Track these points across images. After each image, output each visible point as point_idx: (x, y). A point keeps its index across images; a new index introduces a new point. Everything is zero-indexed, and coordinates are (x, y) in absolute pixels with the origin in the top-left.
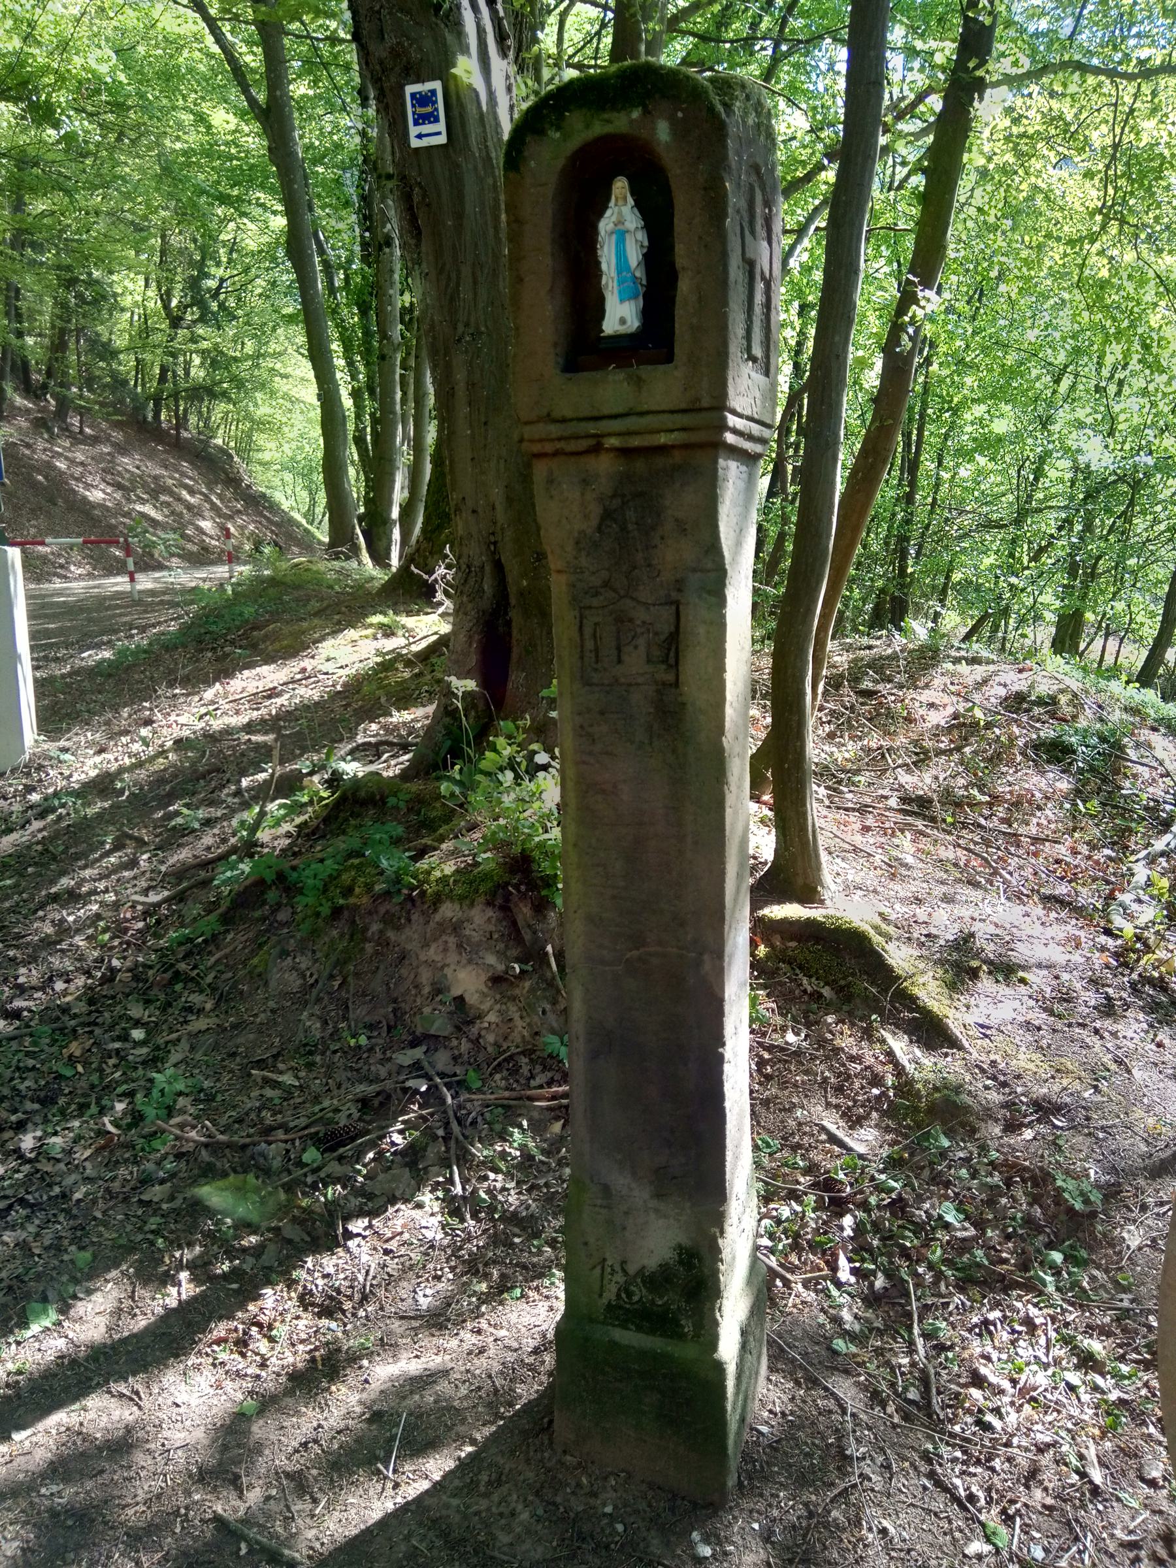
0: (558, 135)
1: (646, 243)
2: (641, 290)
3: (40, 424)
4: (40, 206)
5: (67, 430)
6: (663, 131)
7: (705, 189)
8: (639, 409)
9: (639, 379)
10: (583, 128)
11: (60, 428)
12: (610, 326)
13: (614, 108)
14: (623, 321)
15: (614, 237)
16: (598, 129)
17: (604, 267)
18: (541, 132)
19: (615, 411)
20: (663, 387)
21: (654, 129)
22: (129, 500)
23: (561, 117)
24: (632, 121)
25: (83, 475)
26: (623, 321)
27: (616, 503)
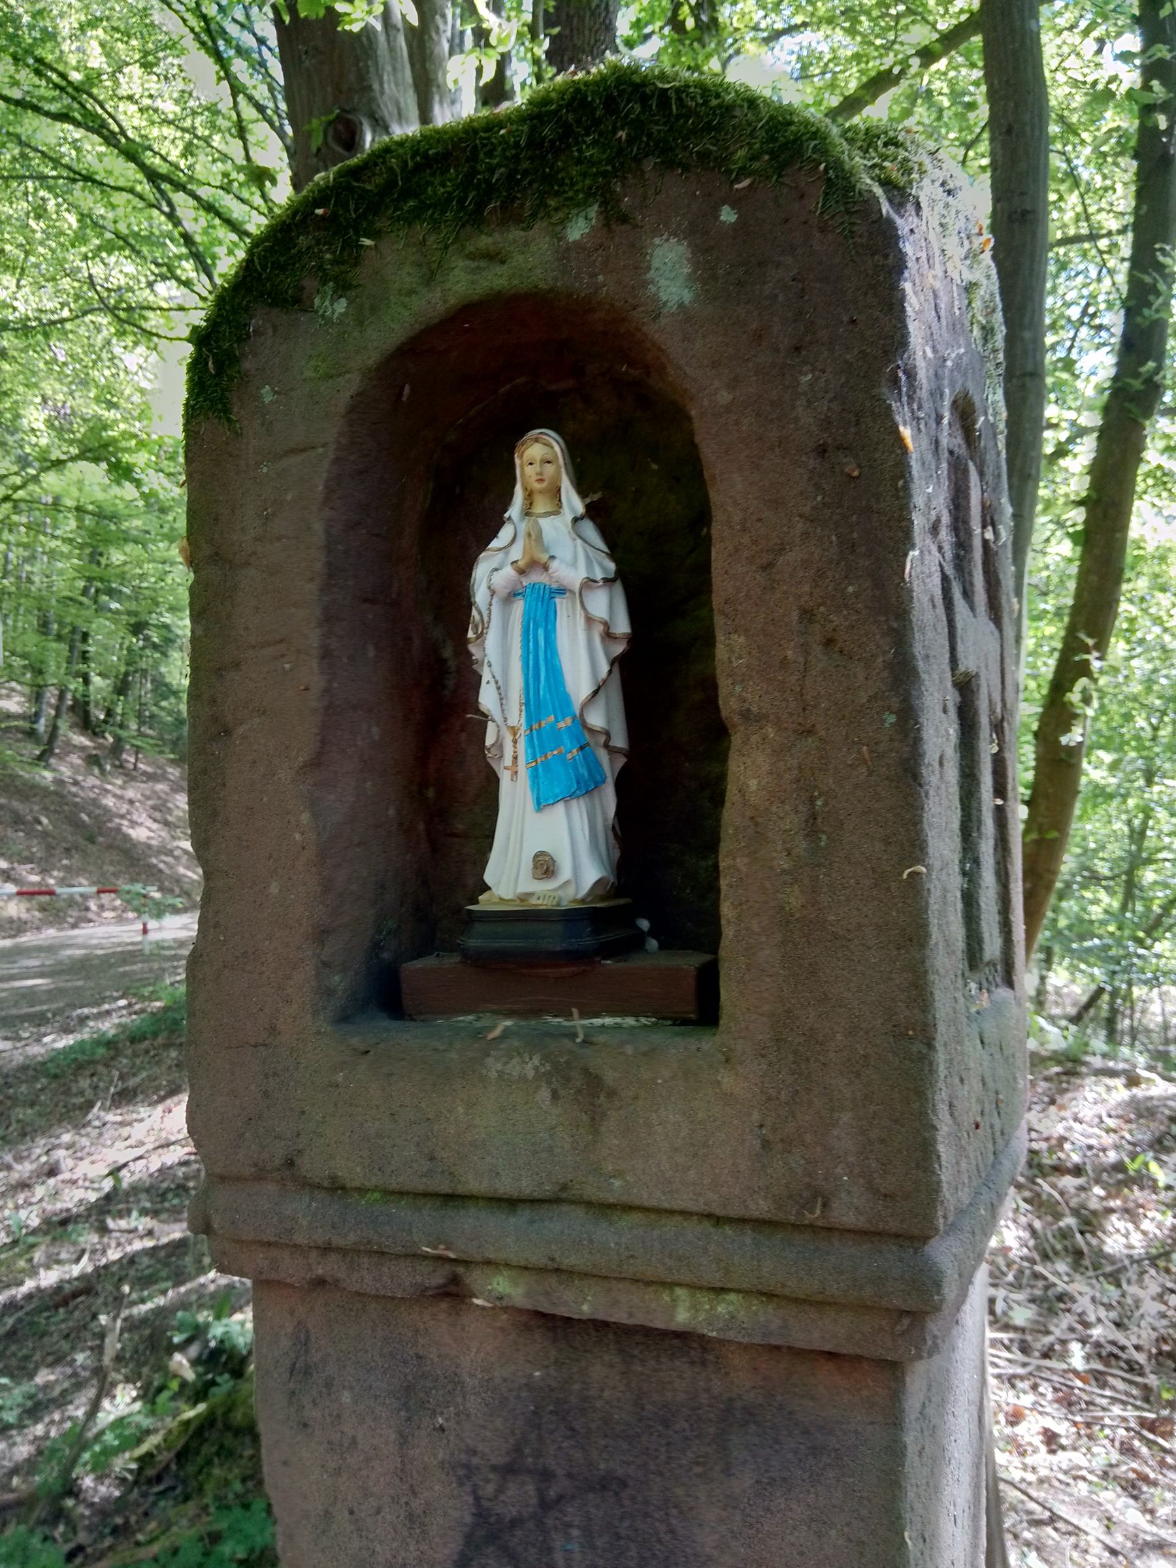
0: (341, 306)
1: (622, 626)
2: (609, 766)
3: (93, 760)
4: (116, 557)
5: (121, 766)
6: (670, 274)
7: (822, 451)
8: (591, 1192)
9: (594, 1084)
10: (416, 284)
11: (114, 766)
12: (507, 878)
13: (511, 216)
14: (545, 866)
15: (519, 607)
16: (463, 281)
17: (487, 698)
18: (298, 302)
19: (506, 1186)
20: (684, 1119)
21: (639, 266)
22: (174, 838)
23: (352, 255)
24: (566, 252)
25: (129, 812)
26: (545, 866)
27: (518, 1497)
